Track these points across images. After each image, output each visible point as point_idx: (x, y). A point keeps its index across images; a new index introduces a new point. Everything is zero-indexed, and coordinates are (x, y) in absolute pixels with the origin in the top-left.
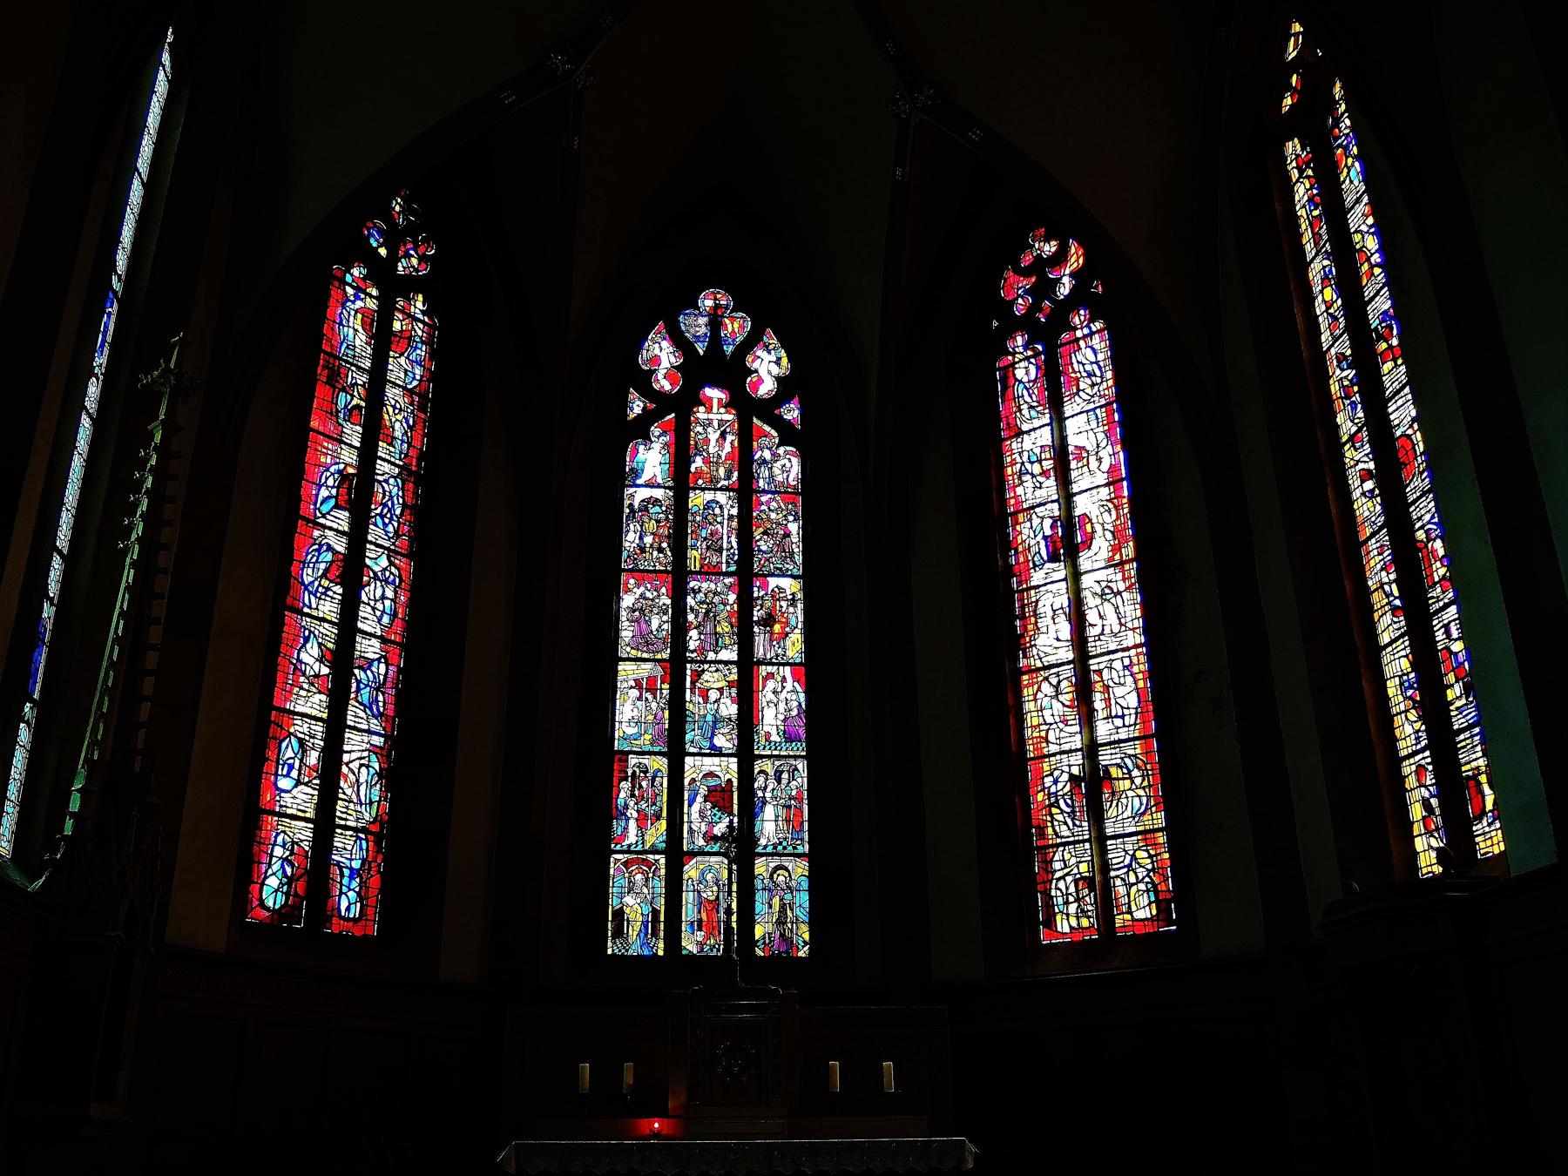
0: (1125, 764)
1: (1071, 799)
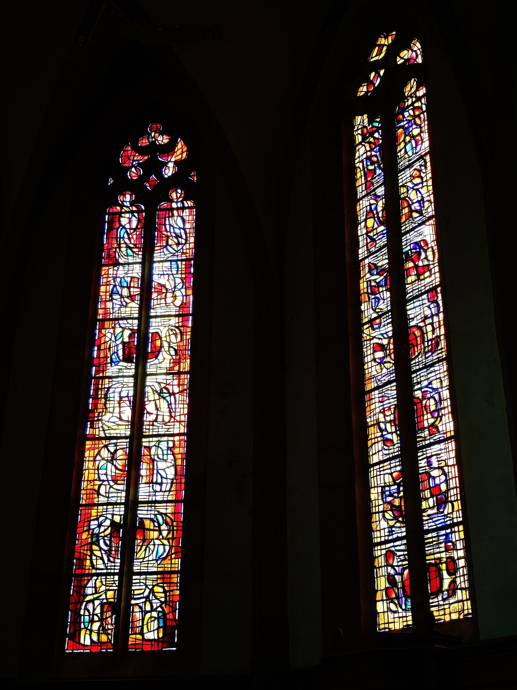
0: (157, 519)
1: (110, 540)
